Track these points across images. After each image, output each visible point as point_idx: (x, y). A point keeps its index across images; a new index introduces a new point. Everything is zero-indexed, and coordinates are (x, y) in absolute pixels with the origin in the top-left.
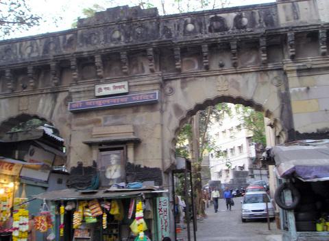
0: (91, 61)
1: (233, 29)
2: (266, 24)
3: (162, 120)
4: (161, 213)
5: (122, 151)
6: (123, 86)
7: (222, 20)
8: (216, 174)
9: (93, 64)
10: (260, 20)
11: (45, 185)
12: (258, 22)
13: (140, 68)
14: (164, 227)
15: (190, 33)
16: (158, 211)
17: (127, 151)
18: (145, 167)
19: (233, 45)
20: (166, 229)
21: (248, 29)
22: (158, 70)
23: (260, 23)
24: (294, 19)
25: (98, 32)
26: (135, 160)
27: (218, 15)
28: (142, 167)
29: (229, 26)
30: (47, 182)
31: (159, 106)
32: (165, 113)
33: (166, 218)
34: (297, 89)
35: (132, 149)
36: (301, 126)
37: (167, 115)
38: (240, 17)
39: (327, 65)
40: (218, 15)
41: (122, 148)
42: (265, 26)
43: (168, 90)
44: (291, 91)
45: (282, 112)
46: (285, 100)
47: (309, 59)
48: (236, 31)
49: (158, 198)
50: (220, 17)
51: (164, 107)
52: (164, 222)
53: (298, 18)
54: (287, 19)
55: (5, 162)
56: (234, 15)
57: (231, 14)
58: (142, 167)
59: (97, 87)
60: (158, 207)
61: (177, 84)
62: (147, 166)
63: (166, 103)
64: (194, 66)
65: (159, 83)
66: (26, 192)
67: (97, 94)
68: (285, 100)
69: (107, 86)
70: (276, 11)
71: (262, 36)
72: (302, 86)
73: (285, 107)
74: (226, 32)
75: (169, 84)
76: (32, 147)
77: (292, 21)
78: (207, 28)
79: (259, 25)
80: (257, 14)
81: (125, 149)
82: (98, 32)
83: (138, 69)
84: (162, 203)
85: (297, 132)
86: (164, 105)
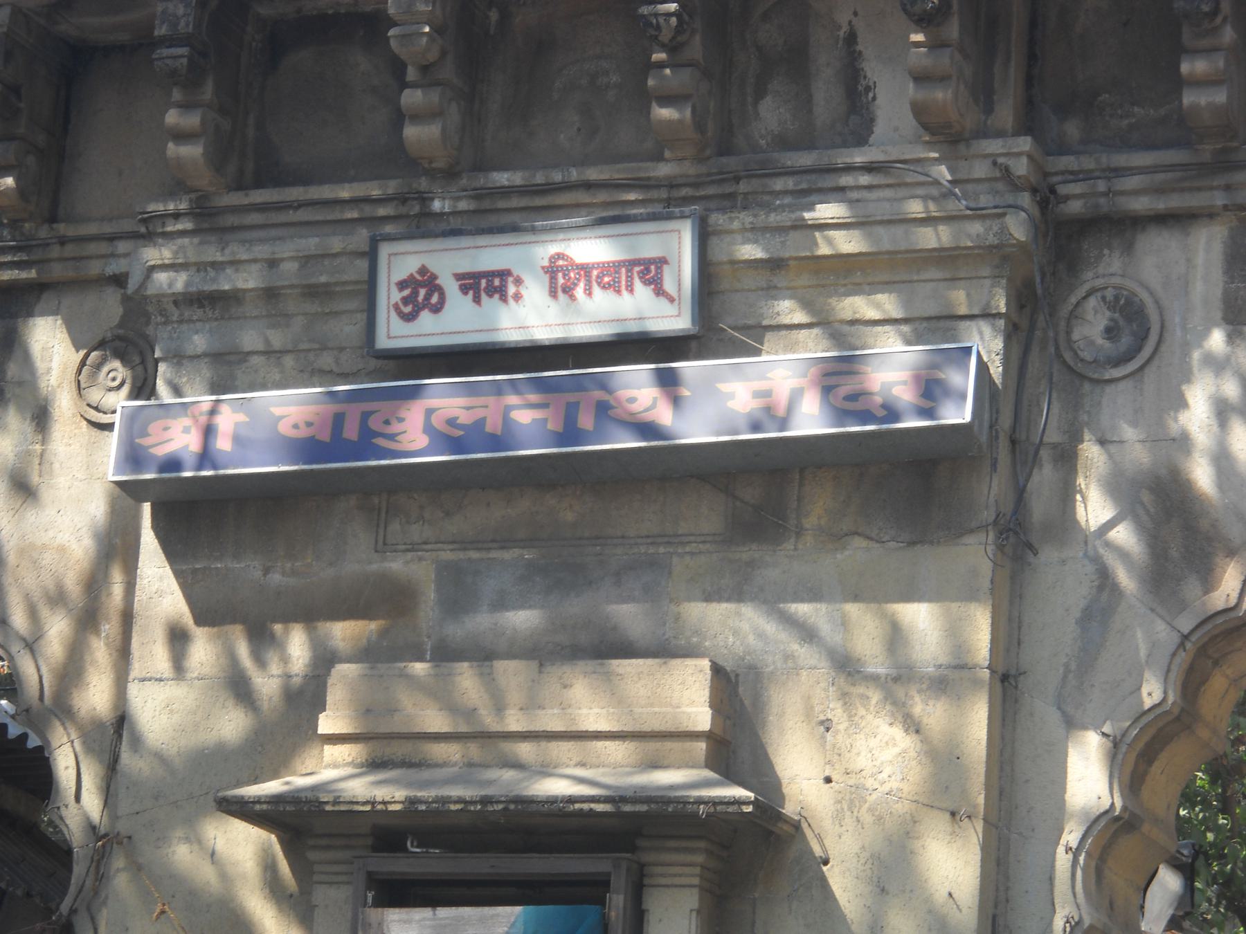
3: (1009, 634)
13: (826, 95)
32: (1048, 555)
36: (392, 335)
43: (1092, 328)
47: (202, 653)
59: (401, 262)
65: (999, 256)
66: (795, 600)
67: (395, 333)
69: (490, 255)
75: (1108, 268)
81: (617, 902)
83: (805, 103)
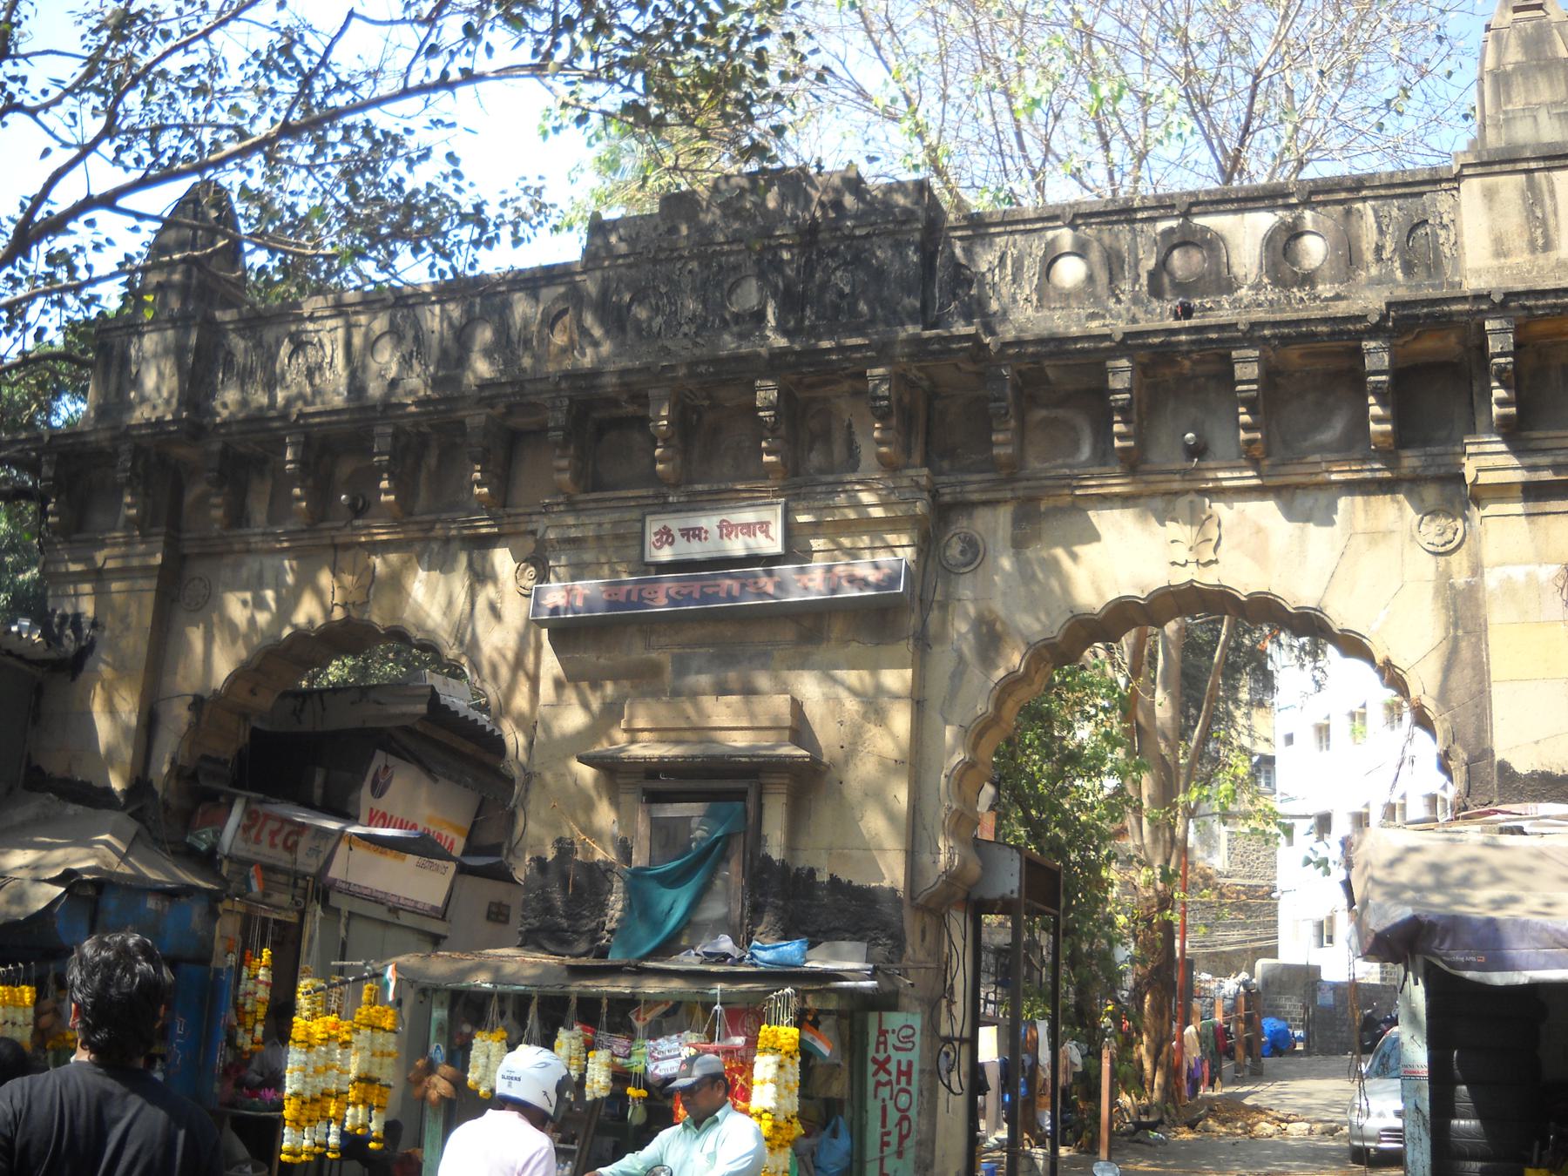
0: (630, 409)
1: (1257, 287)
2: (1408, 268)
4: (883, 1077)
5: (739, 805)
6: (764, 526)
7: (1211, 244)
8: (1310, 931)
9: (643, 422)
10: (1379, 249)
11: (436, 927)
12: (1369, 256)
13: (839, 451)
14: (893, 1139)
15: (1066, 296)
16: (871, 1068)
17: (760, 807)
18: (834, 880)
19: (1245, 361)
20: (900, 1154)
21: (1325, 290)
22: (917, 458)
23: (1379, 259)
24: (1533, 247)
25: (669, 280)
26: (791, 846)
27: (1199, 221)
28: (823, 877)
29: (1238, 270)
30: (442, 914)
31: (913, 621)
32: (936, 649)
33: (903, 1100)
34: (1518, 573)
35: (783, 799)
37: (942, 662)
38: (1293, 233)
39: (326, 1172)
40: (1199, 221)
41: (741, 795)
42: (1399, 275)
43: (955, 550)
44: (1492, 580)
45: (1448, 669)
46: (1464, 614)
48: (1271, 293)
49: (873, 1017)
50: (1205, 229)
51: (933, 627)
52: (893, 1116)
53: (1548, 246)
54: (1500, 251)
55: (267, 817)
56: (1263, 221)
57: (1250, 217)
58: (823, 877)
59: (653, 526)
60: (871, 1053)
61: (995, 524)
62: (844, 878)
63: (944, 607)
64: (1076, 447)
68: (1464, 614)
70: (1456, 207)
71: (1375, 331)
72: (1542, 560)
73: (1466, 653)
74: (1225, 300)
75: (962, 525)
76: (380, 759)
77: (1521, 258)
78: (1144, 280)
79: (1374, 271)
80: (1370, 218)
82: (669, 280)
84: (892, 1039)
85: (1504, 767)
86: (934, 616)
